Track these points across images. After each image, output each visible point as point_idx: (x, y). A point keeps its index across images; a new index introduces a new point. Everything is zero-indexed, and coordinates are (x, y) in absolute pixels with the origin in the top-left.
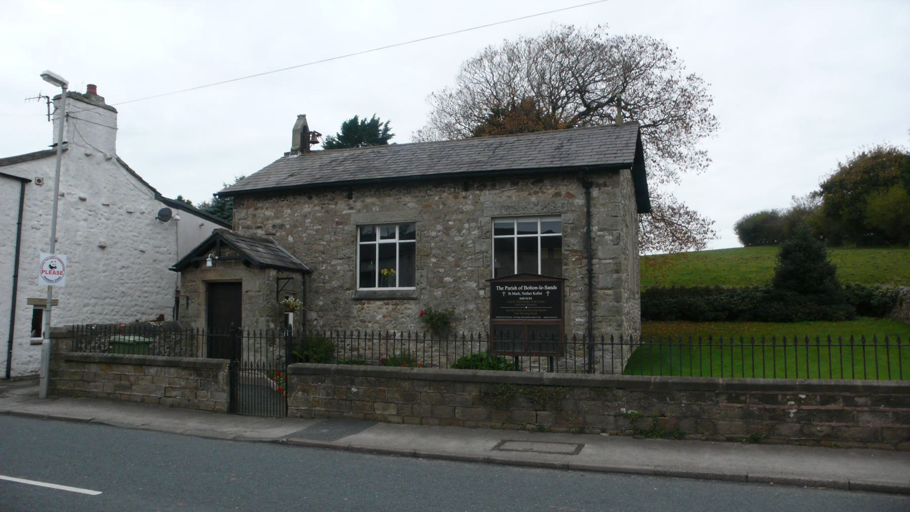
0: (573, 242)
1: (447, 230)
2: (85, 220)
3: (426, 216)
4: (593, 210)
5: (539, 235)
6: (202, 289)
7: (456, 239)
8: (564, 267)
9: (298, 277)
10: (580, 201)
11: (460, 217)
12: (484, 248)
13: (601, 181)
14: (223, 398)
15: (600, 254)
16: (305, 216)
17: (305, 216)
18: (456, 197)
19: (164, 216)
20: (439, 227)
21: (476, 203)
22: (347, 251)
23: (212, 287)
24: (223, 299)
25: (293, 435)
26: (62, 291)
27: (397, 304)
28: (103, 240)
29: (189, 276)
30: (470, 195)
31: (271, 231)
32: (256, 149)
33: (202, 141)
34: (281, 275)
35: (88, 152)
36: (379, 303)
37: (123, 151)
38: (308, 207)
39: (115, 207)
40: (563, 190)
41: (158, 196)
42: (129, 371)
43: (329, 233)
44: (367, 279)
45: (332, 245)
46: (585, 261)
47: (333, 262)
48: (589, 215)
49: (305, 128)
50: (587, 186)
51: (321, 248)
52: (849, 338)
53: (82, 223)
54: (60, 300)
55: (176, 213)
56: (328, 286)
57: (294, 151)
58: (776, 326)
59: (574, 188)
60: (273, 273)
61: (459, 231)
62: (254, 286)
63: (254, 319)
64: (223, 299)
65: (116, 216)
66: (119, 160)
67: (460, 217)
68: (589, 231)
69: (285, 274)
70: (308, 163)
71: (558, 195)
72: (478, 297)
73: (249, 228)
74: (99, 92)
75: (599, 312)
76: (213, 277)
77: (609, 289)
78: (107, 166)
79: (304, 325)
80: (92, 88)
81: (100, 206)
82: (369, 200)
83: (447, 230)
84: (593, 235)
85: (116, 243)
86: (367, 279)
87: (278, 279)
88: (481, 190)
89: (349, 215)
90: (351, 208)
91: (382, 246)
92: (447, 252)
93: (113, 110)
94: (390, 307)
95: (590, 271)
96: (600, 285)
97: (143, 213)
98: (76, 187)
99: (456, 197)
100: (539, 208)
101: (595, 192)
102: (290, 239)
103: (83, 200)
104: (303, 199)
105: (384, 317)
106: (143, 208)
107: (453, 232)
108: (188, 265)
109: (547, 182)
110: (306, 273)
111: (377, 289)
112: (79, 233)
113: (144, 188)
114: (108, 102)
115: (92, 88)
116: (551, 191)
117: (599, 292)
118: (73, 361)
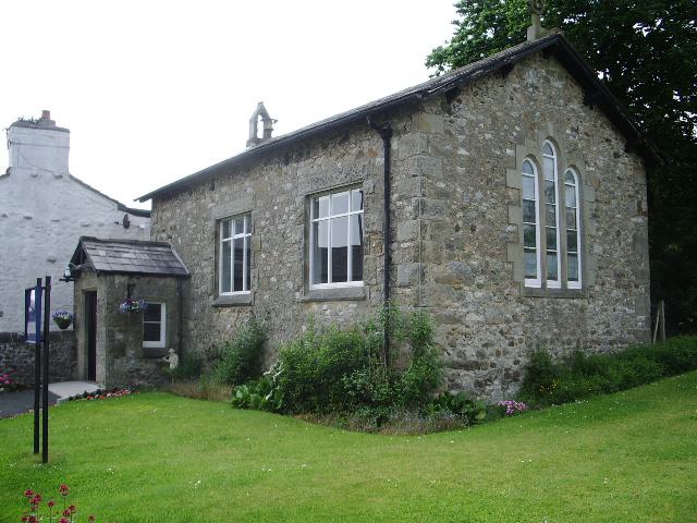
2: (32, 237)
9: (172, 283)
13: (400, 126)
26: (6, 303)
27: (239, 312)
28: (51, 254)
35: (35, 173)
36: (229, 310)
37: (74, 170)
39: (67, 223)
50: (387, 137)
53: (28, 240)
54: (5, 312)
59: (374, 143)
65: (69, 230)
66: (71, 177)
69: (135, 280)
77: (408, 287)
78: (59, 183)
80: (46, 114)
81: (49, 222)
84: (392, 207)
91: (235, 240)
93: (67, 131)
95: (389, 260)
96: (398, 283)
97: (102, 225)
98: (20, 206)
101: (395, 144)
103: (28, 218)
106: (102, 220)
112: (26, 249)
113: (104, 201)
114: (57, 125)
115: (46, 114)
117: (400, 291)
118: (387, 296)
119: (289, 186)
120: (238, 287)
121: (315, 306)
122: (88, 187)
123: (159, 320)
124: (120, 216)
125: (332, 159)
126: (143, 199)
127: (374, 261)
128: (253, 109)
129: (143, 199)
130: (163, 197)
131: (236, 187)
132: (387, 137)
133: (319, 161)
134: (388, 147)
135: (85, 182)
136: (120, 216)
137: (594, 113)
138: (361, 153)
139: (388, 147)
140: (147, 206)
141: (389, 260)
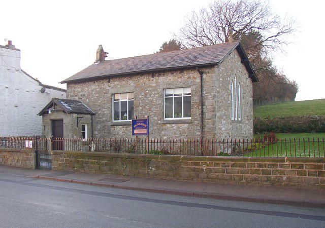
0: (196, 99)
1: (146, 94)
3: (138, 89)
4: (203, 84)
5: (183, 96)
6: (49, 122)
7: (149, 99)
8: (192, 110)
10: (198, 80)
11: (151, 89)
12: (160, 102)
13: (207, 71)
14: (33, 163)
15: (206, 104)
16: (93, 91)
17: (93, 91)
18: (149, 81)
19: (43, 91)
20: (143, 94)
21: (157, 82)
22: (108, 105)
23: (54, 121)
24: (57, 126)
25: (45, 175)
28: (16, 103)
29: (45, 117)
30: (155, 79)
31: (81, 97)
32: (82, 61)
33: (55, 63)
34: (79, 116)
37: (24, 67)
38: (94, 86)
40: (191, 75)
41: (40, 84)
42: (6, 154)
43: (101, 97)
44: (117, 117)
45: (103, 102)
46: (200, 107)
47: (104, 110)
48: (202, 86)
49: (102, 50)
50: (201, 73)
51: (99, 104)
52: (317, 139)
55: (47, 90)
56: (101, 120)
57: (97, 61)
58: (300, 134)
59: (196, 74)
60: (75, 115)
61: (150, 95)
62: (68, 120)
63: (68, 134)
64: (57, 126)
66: (22, 70)
67: (151, 89)
68: (202, 94)
69: (82, 116)
70: (103, 66)
71: (189, 77)
72: (158, 124)
73: (72, 96)
74: (13, 44)
75: (206, 129)
76: (53, 117)
78: (17, 73)
79: (92, 136)
80: (10, 42)
82: (116, 83)
83: (146, 94)
84: (203, 95)
85: (22, 104)
86: (117, 117)
87: (78, 118)
88: (159, 77)
89: (108, 89)
90: (109, 87)
92: (146, 105)
94: (125, 128)
95: (202, 111)
99: (149, 81)
100: (181, 84)
101: (204, 76)
102: (87, 100)
104: (91, 83)
105: (123, 133)
107: (148, 96)
108: (44, 113)
109: (185, 72)
110: (92, 114)
111: (120, 121)
114: (16, 47)
116: (187, 76)
119: (154, 85)
120: (178, 114)
121: (168, 125)
122: (28, 75)
123: (184, 117)
124: (41, 88)
125: (176, 78)
126: (62, 83)
127: (196, 111)
128: (96, 48)
129: (62, 83)
130: (70, 82)
131: (124, 82)
132: (201, 73)
133: (170, 78)
134: (202, 77)
135: (27, 73)
136: (41, 88)
137: (243, 65)
138: (189, 77)
139: (202, 77)
140: (64, 86)
141: (202, 111)
